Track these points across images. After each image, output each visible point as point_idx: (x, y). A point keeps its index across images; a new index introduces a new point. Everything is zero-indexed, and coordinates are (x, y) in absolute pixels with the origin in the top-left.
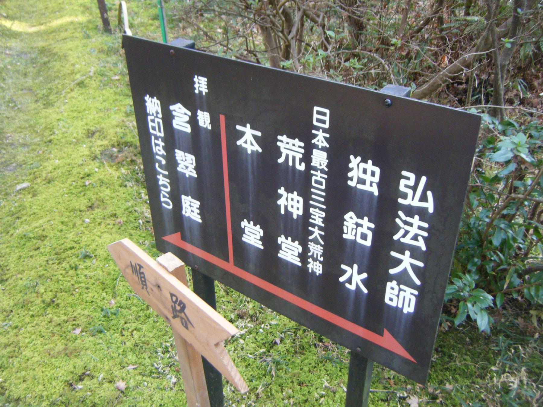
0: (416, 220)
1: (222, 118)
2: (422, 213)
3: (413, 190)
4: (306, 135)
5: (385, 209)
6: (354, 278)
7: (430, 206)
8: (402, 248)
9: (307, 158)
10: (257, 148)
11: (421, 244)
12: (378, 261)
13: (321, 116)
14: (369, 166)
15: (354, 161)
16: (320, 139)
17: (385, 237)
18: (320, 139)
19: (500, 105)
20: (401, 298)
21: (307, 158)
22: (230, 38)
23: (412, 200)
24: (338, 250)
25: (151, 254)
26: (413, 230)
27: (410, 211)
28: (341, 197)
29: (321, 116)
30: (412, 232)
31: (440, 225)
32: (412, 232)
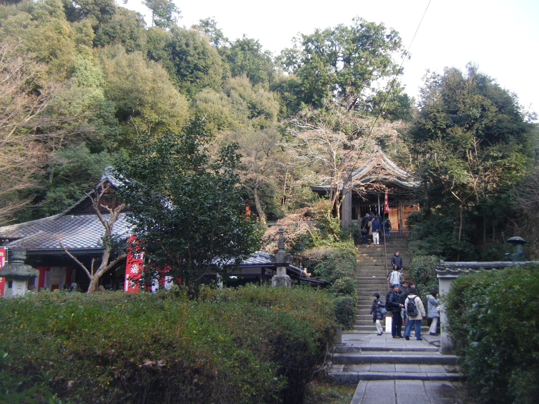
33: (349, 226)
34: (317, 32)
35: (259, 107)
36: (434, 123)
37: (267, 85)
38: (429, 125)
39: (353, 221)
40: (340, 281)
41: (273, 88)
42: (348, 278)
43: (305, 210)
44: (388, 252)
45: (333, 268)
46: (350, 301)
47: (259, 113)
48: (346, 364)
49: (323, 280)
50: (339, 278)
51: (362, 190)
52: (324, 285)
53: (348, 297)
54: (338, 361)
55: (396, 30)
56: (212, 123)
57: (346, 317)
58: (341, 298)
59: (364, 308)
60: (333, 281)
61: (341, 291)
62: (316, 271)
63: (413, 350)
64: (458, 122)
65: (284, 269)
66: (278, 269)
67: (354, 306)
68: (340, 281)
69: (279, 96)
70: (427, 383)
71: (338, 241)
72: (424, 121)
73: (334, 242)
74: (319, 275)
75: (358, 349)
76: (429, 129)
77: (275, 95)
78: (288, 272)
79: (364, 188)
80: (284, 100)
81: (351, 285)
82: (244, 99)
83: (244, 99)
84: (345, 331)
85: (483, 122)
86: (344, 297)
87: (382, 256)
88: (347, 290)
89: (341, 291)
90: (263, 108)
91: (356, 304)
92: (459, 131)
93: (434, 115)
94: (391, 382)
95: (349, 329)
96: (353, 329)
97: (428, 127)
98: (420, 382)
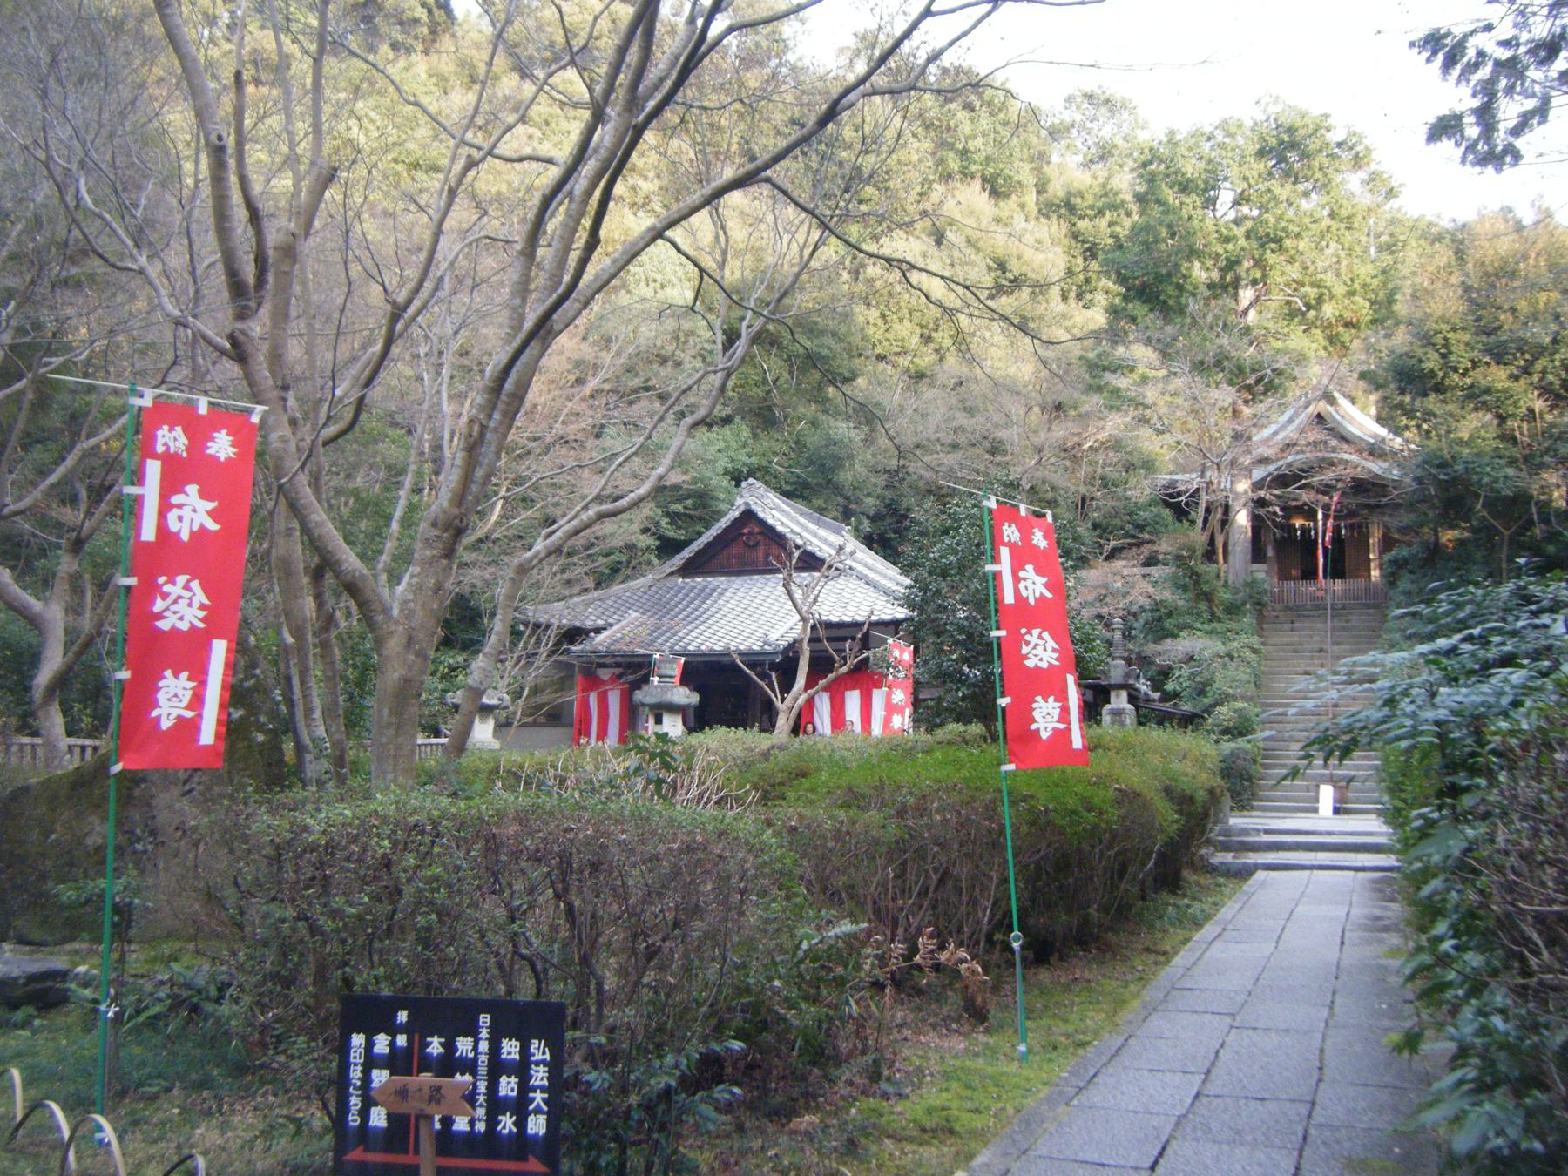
0: (541, 1068)
1: (417, 1037)
2: (544, 1062)
3: (539, 1050)
4: (473, 1032)
5: (522, 1069)
6: (507, 1123)
7: (547, 1056)
8: (534, 1089)
9: (475, 1048)
10: (441, 1050)
11: (546, 1082)
12: (520, 1107)
13: (485, 1020)
14: (514, 1042)
15: (505, 1042)
16: (484, 1033)
17: (525, 1088)
18: (484, 1033)
19: (721, 514)
20: (537, 1125)
21: (475, 1048)
22: (503, 128)
23: (538, 1057)
24: (496, 1106)
25: (232, 680)
26: (541, 1075)
27: (537, 1063)
28: (497, 1067)
29: (485, 1020)
30: (540, 1076)
31: (555, 1067)
32: (540, 1076)
33: (1246, 584)
34: (1172, 133)
35: (1015, 268)
36: (1443, 356)
37: (1031, 198)
38: (1432, 362)
39: (1256, 567)
40: (1224, 709)
41: (1048, 209)
42: (1240, 705)
43: (1146, 550)
44: (1334, 643)
45: (1208, 683)
46: (1246, 752)
47: (1016, 283)
48: (1236, 851)
49: (1186, 707)
50: (1222, 704)
51: (1275, 513)
52: (1189, 721)
53: (1241, 743)
54: (1226, 847)
55: (1358, 130)
56: (906, 323)
57: (1241, 784)
58: (1228, 746)
59: (1276, 766)
60: (1209, 710)
61: (1226, 731)
62: (1169, 687)
63: (1352, 834)
64: (1499, 355)
65: (1124, 694)
66: (1113, 695)
67: (1255, 761)
68: (1224, 712)
69: (1064, 232)
70: (1361, 875)
71: (1219, 620)
72: (1419, 352)
73: (1210, 621)
74: (1176, 695)
75: (1258, 831)
76: (1432, 371)
77: (1054, 228)
78: (1132, 699)
79: (1277, 509)
80: (1078, 241)
81: (1248, 720)
82: (978, 250)
83: (978, 250)
84: (1236, 813)
85: (1557, 356)
86: (1232, 745)
87: (1321, 651)
88: (1239, 729)
89: (1226, 731)
90: (1024, 269)
91: (1259, 760)
92: (1498, 377)
93: (1446, 339)
94: (1307, 872)
95: (1243, 808)
96: (1252, 808)
97: (1428, 365)
98: (1351, 873)
